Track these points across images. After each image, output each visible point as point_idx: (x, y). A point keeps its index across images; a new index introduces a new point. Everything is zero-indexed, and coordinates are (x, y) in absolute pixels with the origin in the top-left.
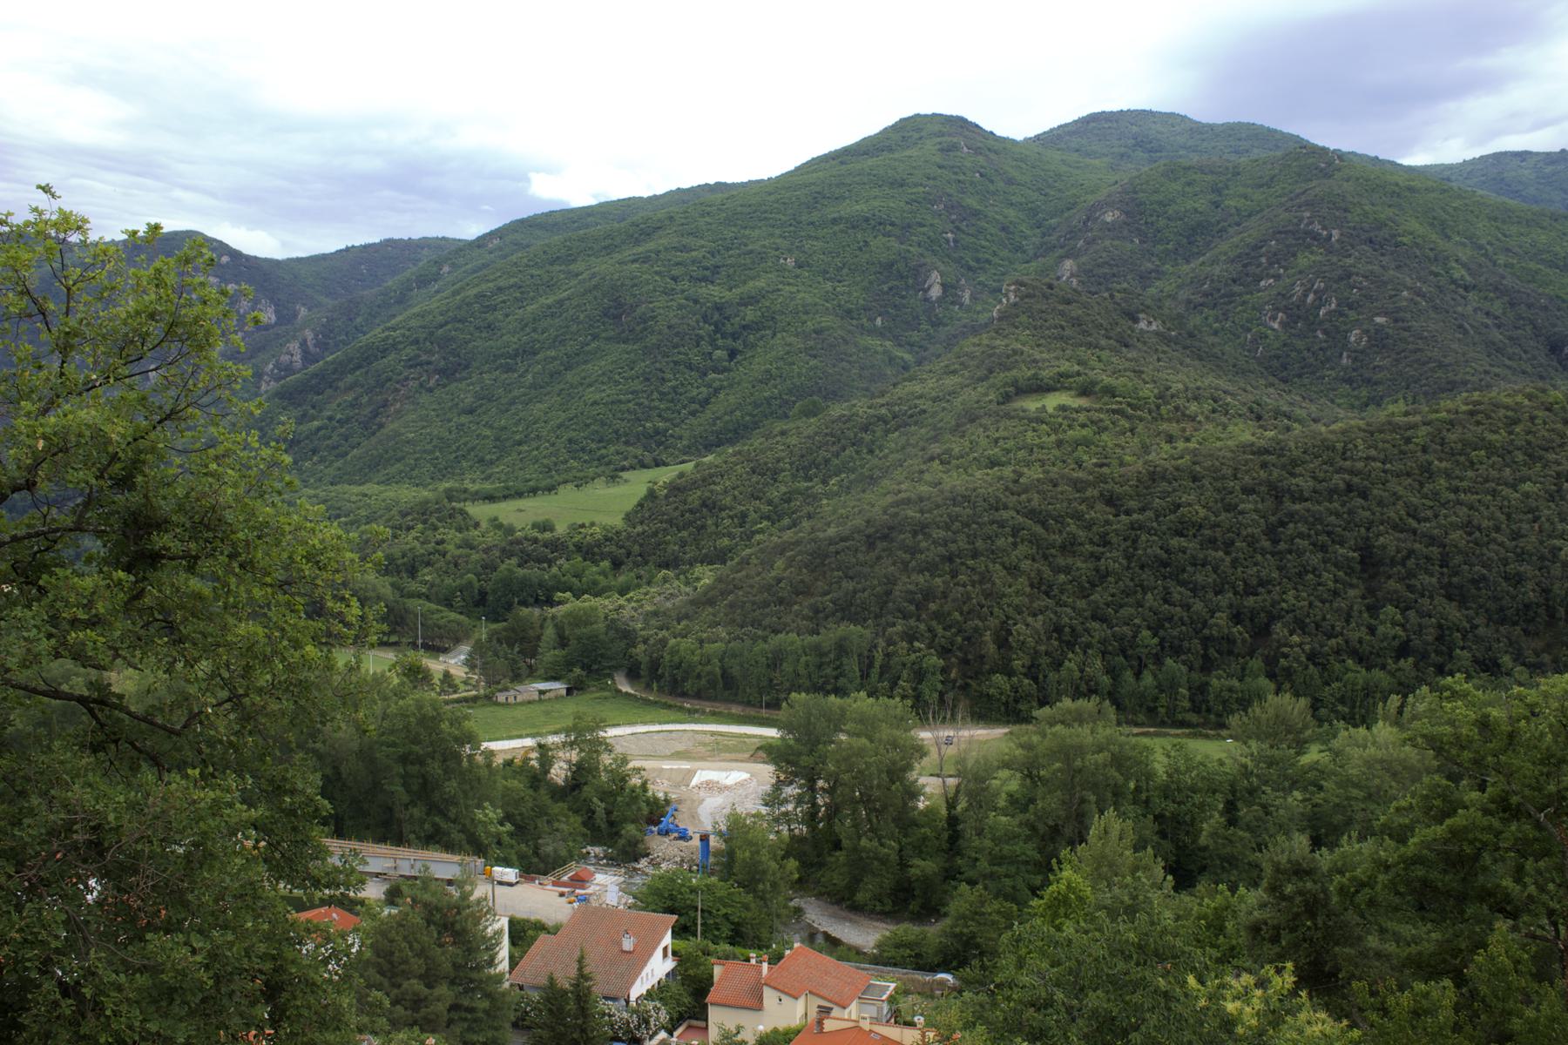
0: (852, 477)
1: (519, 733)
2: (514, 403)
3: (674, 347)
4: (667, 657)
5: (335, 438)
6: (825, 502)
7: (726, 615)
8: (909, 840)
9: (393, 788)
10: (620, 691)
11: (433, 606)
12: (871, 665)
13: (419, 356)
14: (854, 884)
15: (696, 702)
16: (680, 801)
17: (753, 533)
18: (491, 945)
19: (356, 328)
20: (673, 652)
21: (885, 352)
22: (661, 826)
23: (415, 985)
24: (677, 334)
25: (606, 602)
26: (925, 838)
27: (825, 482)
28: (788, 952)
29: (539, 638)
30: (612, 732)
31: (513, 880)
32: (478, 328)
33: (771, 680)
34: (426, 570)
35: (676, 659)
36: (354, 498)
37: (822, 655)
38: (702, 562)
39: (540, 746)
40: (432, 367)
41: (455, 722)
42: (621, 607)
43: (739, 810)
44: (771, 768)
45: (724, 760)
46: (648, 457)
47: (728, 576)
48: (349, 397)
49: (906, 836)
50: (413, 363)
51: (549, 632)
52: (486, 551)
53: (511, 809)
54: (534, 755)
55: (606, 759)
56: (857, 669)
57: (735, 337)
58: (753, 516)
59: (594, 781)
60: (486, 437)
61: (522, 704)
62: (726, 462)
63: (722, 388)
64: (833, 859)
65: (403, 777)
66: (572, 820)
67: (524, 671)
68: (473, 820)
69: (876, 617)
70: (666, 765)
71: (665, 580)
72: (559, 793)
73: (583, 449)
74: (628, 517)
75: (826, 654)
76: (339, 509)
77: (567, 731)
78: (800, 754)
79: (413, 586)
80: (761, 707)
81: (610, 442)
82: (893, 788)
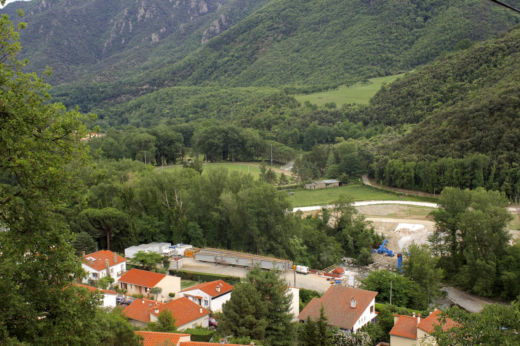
0: (485, 79)
1: (316, 203)
2: (318, 46)
3: (396, 16)
4: (387, 168)
5: (235, 65)
6: (470, 92)
7: (417, 148)
8: (502, 261)
9: (253, 228)
10: (365, 184)
11: (278, 144)
12: (489, 174)
13: (273, 25)
14: (473, 282)
15: (401, 190)
16: (389, 238)
17: (433, 108)
18: (288, 301)
19: (244, 12)
20: (390, 167)
21: (506, 14)
22: (379, 249)
23: (250, 318)
24: (398, 9)
25: (360, 142)
26: (510, 261)
27: (470, 82)
28: (431, 313)
29: (326, 159)
30: (357, 204)
31: (306, 271)
32: (301, 11)
33: (438, 180)
34: (275, 127)
35: (392, 169)
36: (244, 93)
37: (465, 168)
38: (407, 122)
39: (324, 210)
40: (279, 30)
41: (281, 198)
42: (367, 144)
43: (416, 242)
44: (433, 223)
45: (413, 219)
46: (382, 72)
47: (419, 129)
48: (241, 46)
49: (500, 259)
50: (270, 29)
51: (331, 156)
52: (304, 117)
53: (307, 239)
54: (321, 214)
55: (354, 217)
56: (482, 176)
57: (427, 10)
58: (433, 99)
59: (349, 227)
60: (305, 63)
61: (318, 190)
62: (420, 73)
63: (420, 36)
64: (462, 269)
65: (257, 223)
66: (336, 245)
67: (319, 174)
68: (289, 243)
69: (493, 150)
70: (384, 220)
71: (389, 131)
72: (331, 232)
73: (351, 68)
74: (371, 101)
75: (466, 168)
76: (237, 98)
77: (336, 203)
78: (448, 217)
79: (269, 134)
80: (433, 193)
81: (364, 64)
82: (494, 235)
